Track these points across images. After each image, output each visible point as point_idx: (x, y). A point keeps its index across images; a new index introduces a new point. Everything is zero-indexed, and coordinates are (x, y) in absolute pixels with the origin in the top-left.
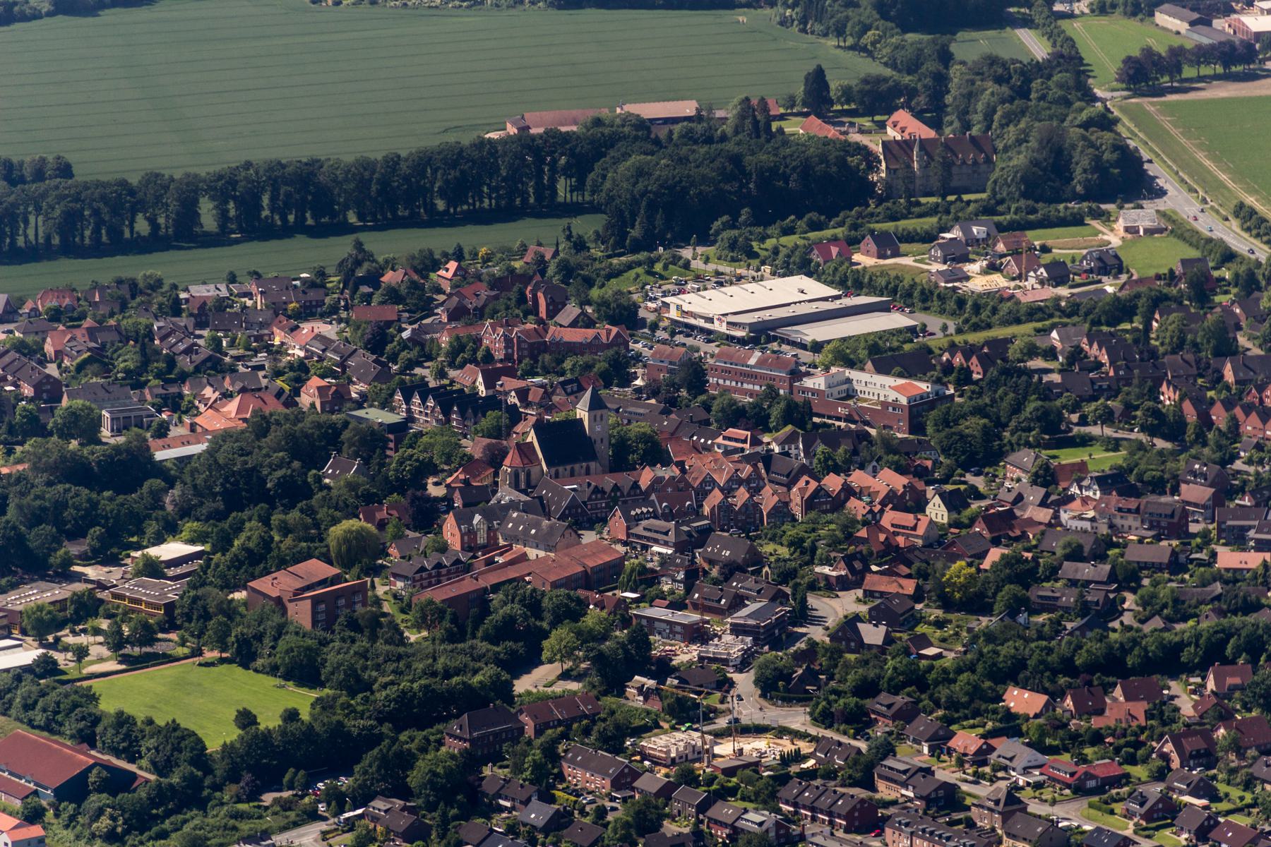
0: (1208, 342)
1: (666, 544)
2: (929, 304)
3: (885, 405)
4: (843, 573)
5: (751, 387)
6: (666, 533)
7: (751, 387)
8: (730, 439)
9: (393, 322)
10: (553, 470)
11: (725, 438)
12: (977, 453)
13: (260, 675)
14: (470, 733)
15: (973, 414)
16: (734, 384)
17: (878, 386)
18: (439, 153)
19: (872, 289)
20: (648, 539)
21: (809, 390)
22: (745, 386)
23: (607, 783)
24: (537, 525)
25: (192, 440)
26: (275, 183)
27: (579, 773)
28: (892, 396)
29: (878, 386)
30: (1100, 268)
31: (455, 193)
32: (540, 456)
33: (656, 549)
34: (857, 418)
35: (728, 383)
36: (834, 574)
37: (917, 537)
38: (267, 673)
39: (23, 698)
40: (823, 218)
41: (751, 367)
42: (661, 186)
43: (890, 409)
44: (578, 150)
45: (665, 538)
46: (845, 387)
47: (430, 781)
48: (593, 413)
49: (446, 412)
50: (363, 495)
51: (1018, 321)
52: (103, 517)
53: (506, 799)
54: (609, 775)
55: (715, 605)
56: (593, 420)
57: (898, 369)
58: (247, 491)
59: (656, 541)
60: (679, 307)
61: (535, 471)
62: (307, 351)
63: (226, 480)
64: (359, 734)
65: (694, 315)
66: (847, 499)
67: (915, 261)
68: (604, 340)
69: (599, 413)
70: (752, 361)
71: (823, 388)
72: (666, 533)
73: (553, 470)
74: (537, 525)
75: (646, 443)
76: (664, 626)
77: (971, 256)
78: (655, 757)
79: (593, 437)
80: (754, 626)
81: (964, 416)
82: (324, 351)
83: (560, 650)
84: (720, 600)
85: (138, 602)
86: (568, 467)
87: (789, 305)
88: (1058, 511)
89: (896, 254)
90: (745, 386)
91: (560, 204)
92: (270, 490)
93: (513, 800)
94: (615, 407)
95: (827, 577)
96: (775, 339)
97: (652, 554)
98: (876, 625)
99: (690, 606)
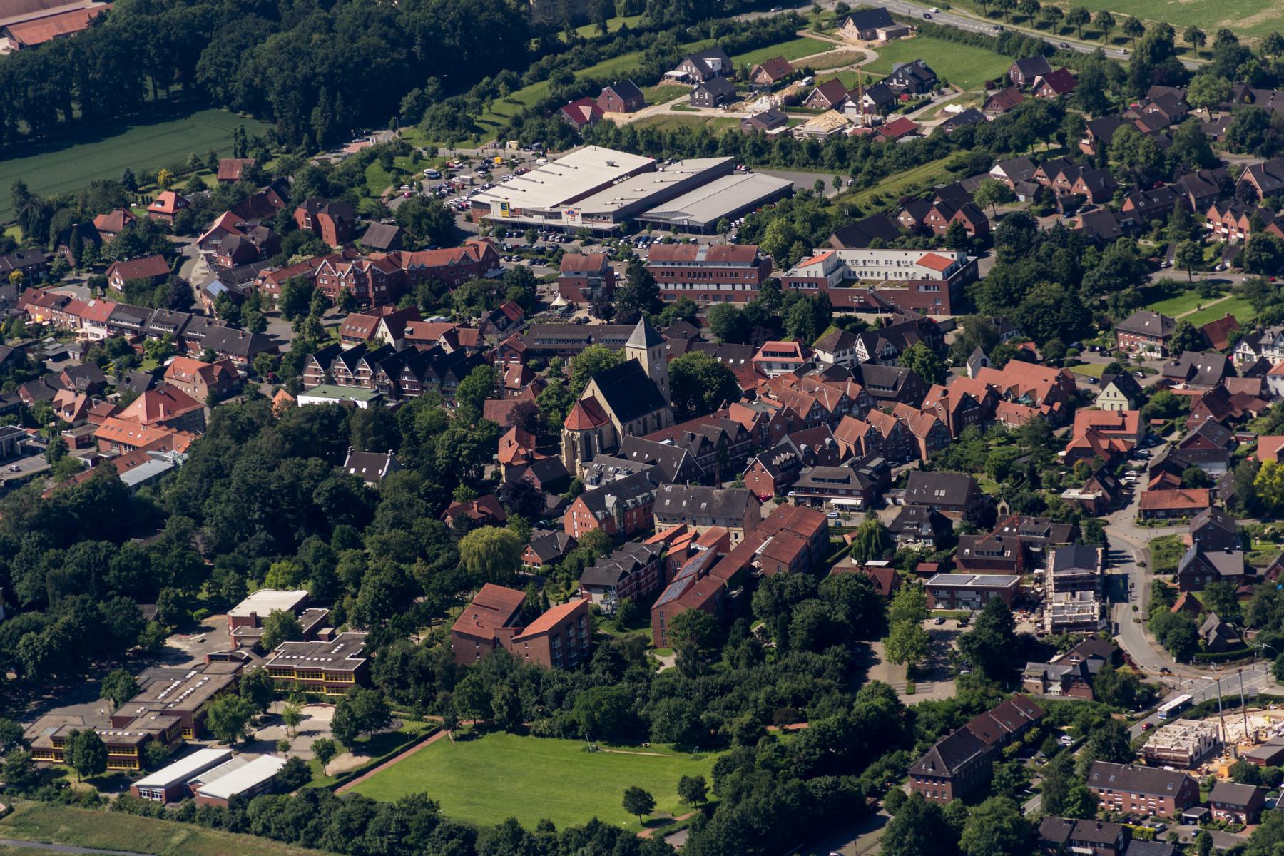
0: (1189, 153)
1: (849, 494)
2: (766, 157)
3: (913, 284)
4: (1099, 494)
5: (704, 287)
6: (847, 481)
7: (704, 287)
8: (773, 354)
9: (166, 275)
10: (627, 425)
11: (765, 354)
12: (1070, 324)
13: (549, 741)
14: (950, 770)
15: (1037, 279)
16: (680, 287)
17: (882, 263)
18: (23, 65)
19: (710, 149)
20: (822, 491)
21: (803, 281)
22: (696, 287)
23: (1169, 802)
24: (707, 497)
25: (136, 460)
26: (822, 165)
27: (1119, 797)
28: (920, 272)
29: (882, 263)
30: (918, 85)
31: (39, 112)
32: (608, 410)
33: (835, 501)
34: (875, 304)
35: (671, 287)
36: (1090, 497)
37: (1129, 436)
38: (559, 736)
39: (342, 822)
40: (515, 74)
41: (702, 263)
42: (332, 66)
43: (922, 289)
44: (173, 38)
45: (846, 486)
46: (840, 271)
47: (1000, 841)
48: (651, 349)
49: (394, 374)
50: (427, 494)
51: (917, 162)
52: (159, 574)
53: (1082, 844)
54: (1169, 793)
55: (998, 558)
56: (652, 357)
57: (878, 239)
58: (291, 512)
59: (835, 493)
60: (504, 206)
61: (606, 430)
62: (110, 327)
63: (264, 504)
64: (825, 796)
65: (530, 213)
66: (996, 405)
67: (673, 108)
68: (474, 258)
69: (657, 348)
70: (701, 257)
71: (821, 275)
72: (847, 481)
73: (627, 425)
74: (707, 497)
75: (720, 375)
76: (973, 594)
77: (739, 94)
78: (1176, 759)
79: (656, 378)
80: (1088, 577)
81: (1028, 284)
82: (142, 324)
83: (912, 647)
84: (1002, 553)
85: (317, 673)
86: (641, 419)
87: (609, 184)
88: (1264, 380)
89: (642, 105)
90: (696, 287)
91: (149, 103)
92: (319, 506)
93: (1093, 844)
94: (586, 337)
95: (1081, 503)
96: (644, 225)
97: (831, 509)
98: (1229, 552)
99: (959, 564)
